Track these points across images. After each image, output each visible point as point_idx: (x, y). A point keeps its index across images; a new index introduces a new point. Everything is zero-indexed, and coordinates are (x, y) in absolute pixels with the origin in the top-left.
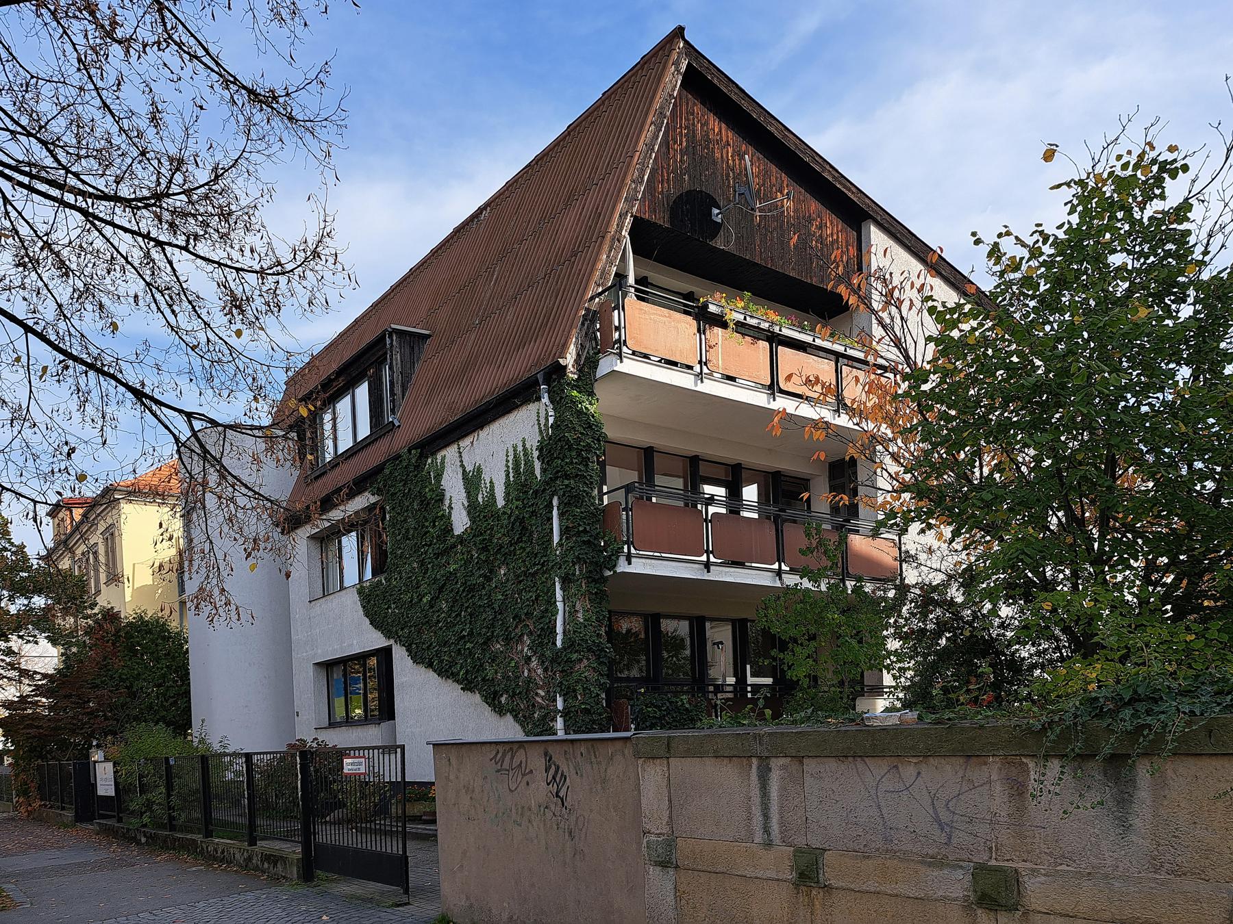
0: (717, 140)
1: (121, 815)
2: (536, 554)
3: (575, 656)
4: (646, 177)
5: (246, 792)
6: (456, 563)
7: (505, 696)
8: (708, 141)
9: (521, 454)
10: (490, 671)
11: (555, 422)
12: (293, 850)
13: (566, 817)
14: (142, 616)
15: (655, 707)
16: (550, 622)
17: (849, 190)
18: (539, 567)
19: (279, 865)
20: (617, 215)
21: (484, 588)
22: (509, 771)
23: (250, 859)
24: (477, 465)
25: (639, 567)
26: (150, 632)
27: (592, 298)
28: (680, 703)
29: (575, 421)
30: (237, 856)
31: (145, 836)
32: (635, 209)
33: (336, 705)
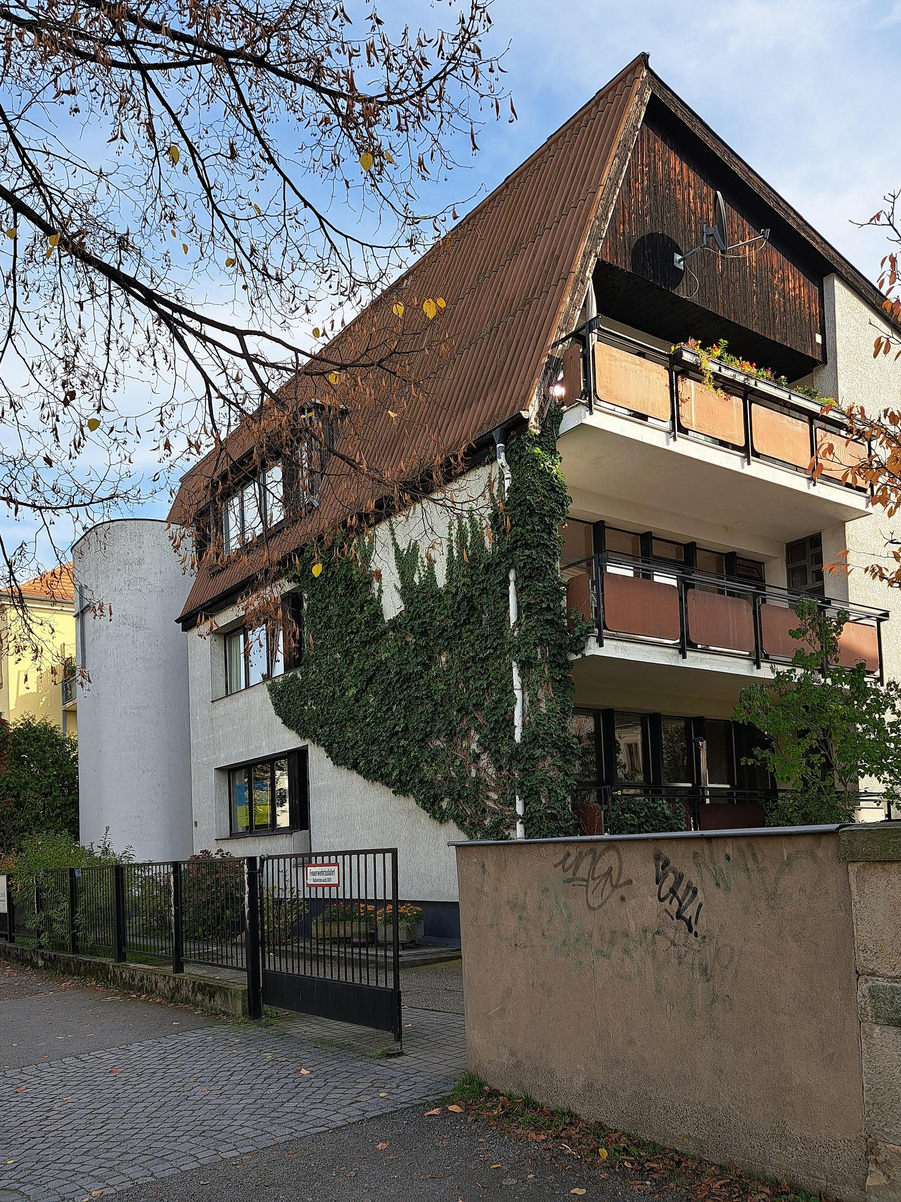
0: (678, 180)
1: (13, 934)
2: (487, 637)
3: (538, 752)
4: (610, 215)
5: (173, 909)
6: (387, 650)
7: (446, 800)
8: (669, 180)
9: (468, 526)
10: (427, 771)
11: (513, 485)
12: (239, 981)
13: (696, 947)
14: (30, 723)
15: (633, 812)
16: (506, 713)
17: (814, 239)
18: (492, 651)
19: (217, 997)
20: (580, 254)
21: (421, 677)
22: (587, 881)
23: (177, 988)
24: (413, 541)
25: (612, 649)
26: (37, 739)
27: (555, 345)
28: (659, 809)
29: (538, 483)
30: (161, 985)
31: (43, 959)
32: (599, 248)
33: (239, 814)
